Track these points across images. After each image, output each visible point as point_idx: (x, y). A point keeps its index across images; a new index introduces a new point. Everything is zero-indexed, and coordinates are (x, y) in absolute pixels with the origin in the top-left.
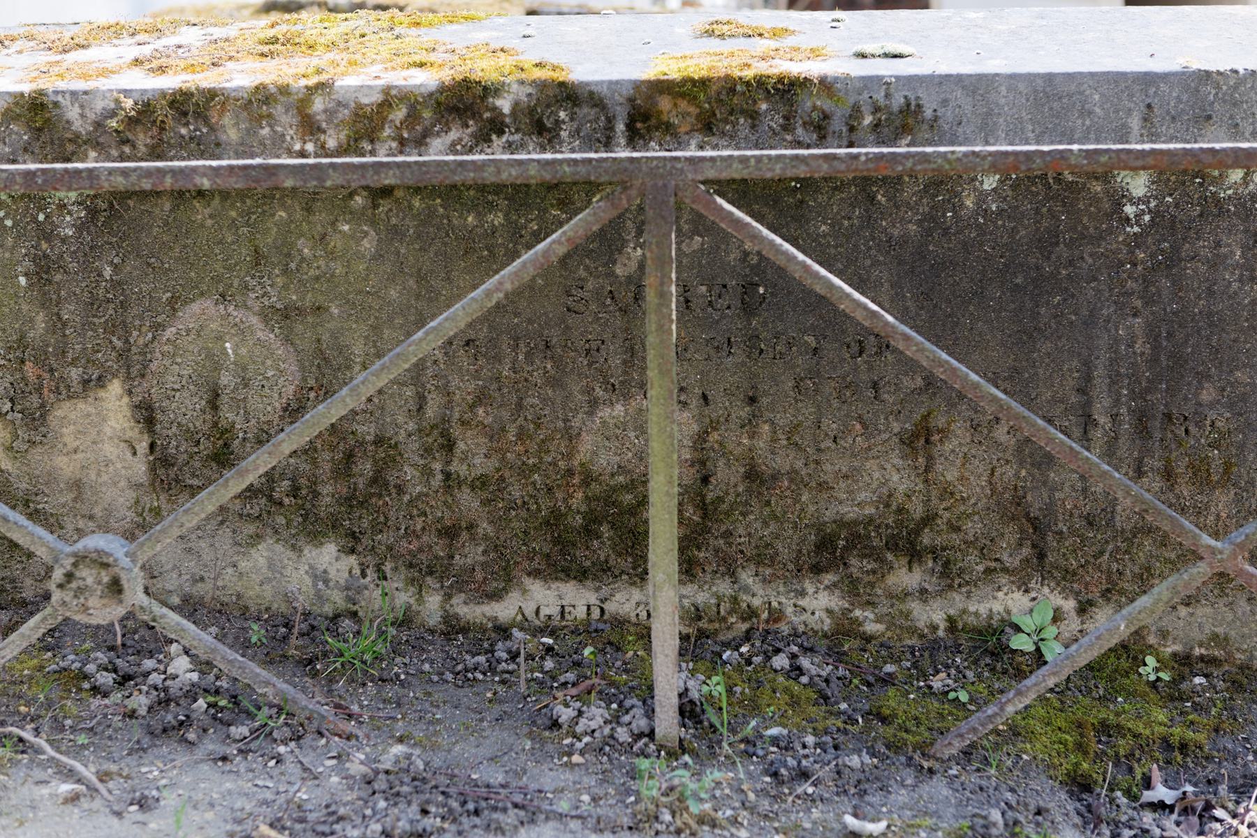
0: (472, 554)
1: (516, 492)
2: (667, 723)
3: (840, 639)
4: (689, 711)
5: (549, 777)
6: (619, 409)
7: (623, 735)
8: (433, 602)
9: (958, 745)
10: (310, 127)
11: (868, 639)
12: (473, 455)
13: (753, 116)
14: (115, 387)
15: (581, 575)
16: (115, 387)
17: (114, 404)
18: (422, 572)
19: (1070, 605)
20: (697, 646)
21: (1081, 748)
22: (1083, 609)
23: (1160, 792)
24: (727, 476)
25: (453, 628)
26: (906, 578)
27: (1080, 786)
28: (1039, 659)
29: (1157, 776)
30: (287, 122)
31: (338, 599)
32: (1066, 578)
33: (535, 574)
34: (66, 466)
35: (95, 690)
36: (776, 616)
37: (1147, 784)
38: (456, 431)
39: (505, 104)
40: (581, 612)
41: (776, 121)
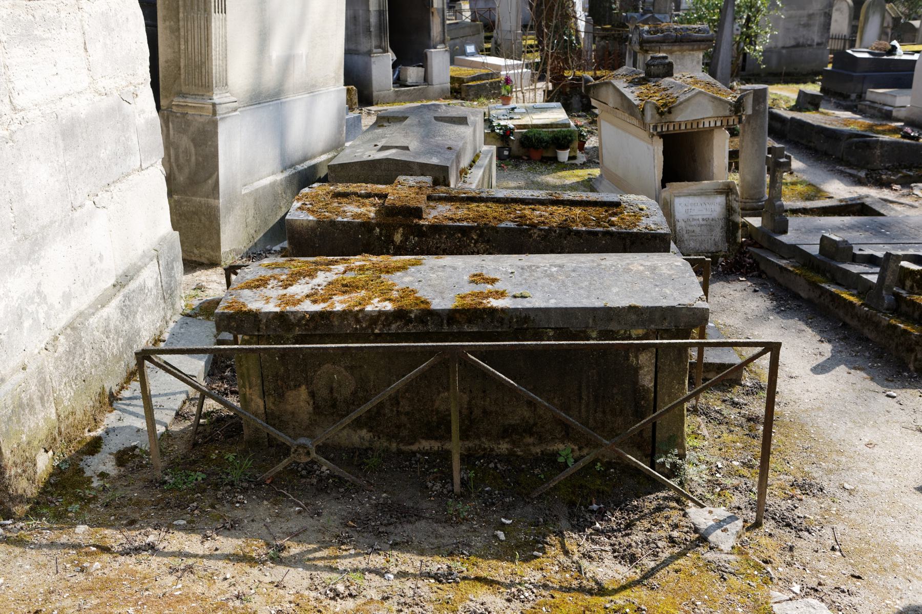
0: (404, 433)
1: (417, 416)
2: (457, 488)
3: (508, 458)
4: (463, 483)
5: (425, 504)
6: (446, 394)
7: (445, 491)
8: (394, 445)
9: (537, 495)
10: (358, 321)
11: (518, 456)
12: (405, 406)
13: (483, 319)
14: (304, 387)
15: (436, 439)
16: (304, 387)
17: (303, 391)
18: (391, 437)
19: (576, 448)
20: (468, 459)
21: (573, 493)
22: (580, 449)
23: (595, 507)
24: (477, 412)
25: (400, 452)
26: (530, 440)
27: (572, 504)
28: (567, 466)
29: (594, 501)
30: (352, 321)
31: (367, 444)
32: (575, 441)
33: (423, 438)
34: (289, 408)
35: (302, 477)
36: (492, 450)
37: (591, 504)
38: (400, 399)
39: (413, 316)
40: (436, 448)
41: (489, 320)
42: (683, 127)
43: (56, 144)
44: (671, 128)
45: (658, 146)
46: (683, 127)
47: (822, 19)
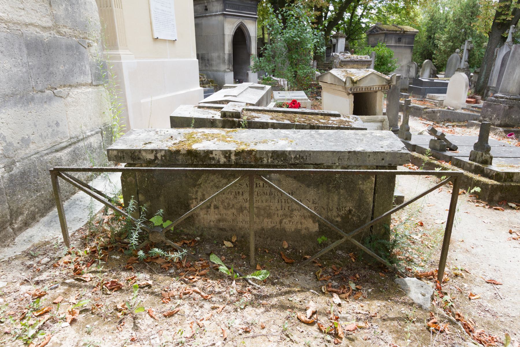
42: (364, 90)
43: (20, 49)
44: (358, 90)
45: (352, 97)
46: (364, 90)
47: (407, 68)
